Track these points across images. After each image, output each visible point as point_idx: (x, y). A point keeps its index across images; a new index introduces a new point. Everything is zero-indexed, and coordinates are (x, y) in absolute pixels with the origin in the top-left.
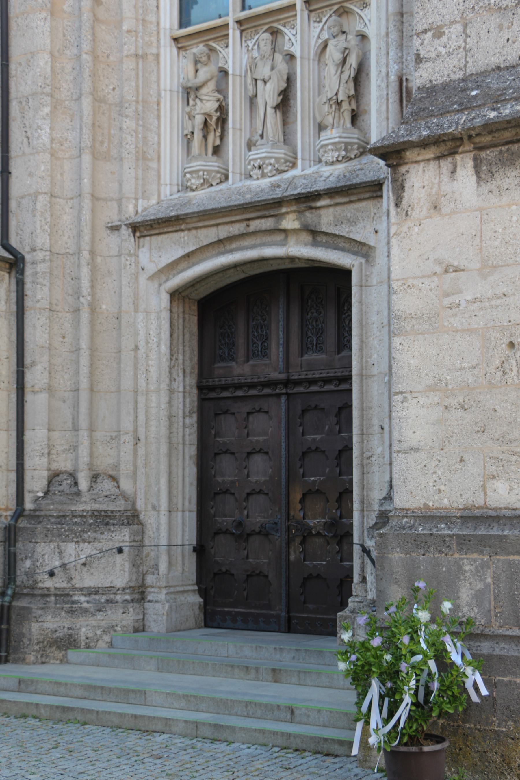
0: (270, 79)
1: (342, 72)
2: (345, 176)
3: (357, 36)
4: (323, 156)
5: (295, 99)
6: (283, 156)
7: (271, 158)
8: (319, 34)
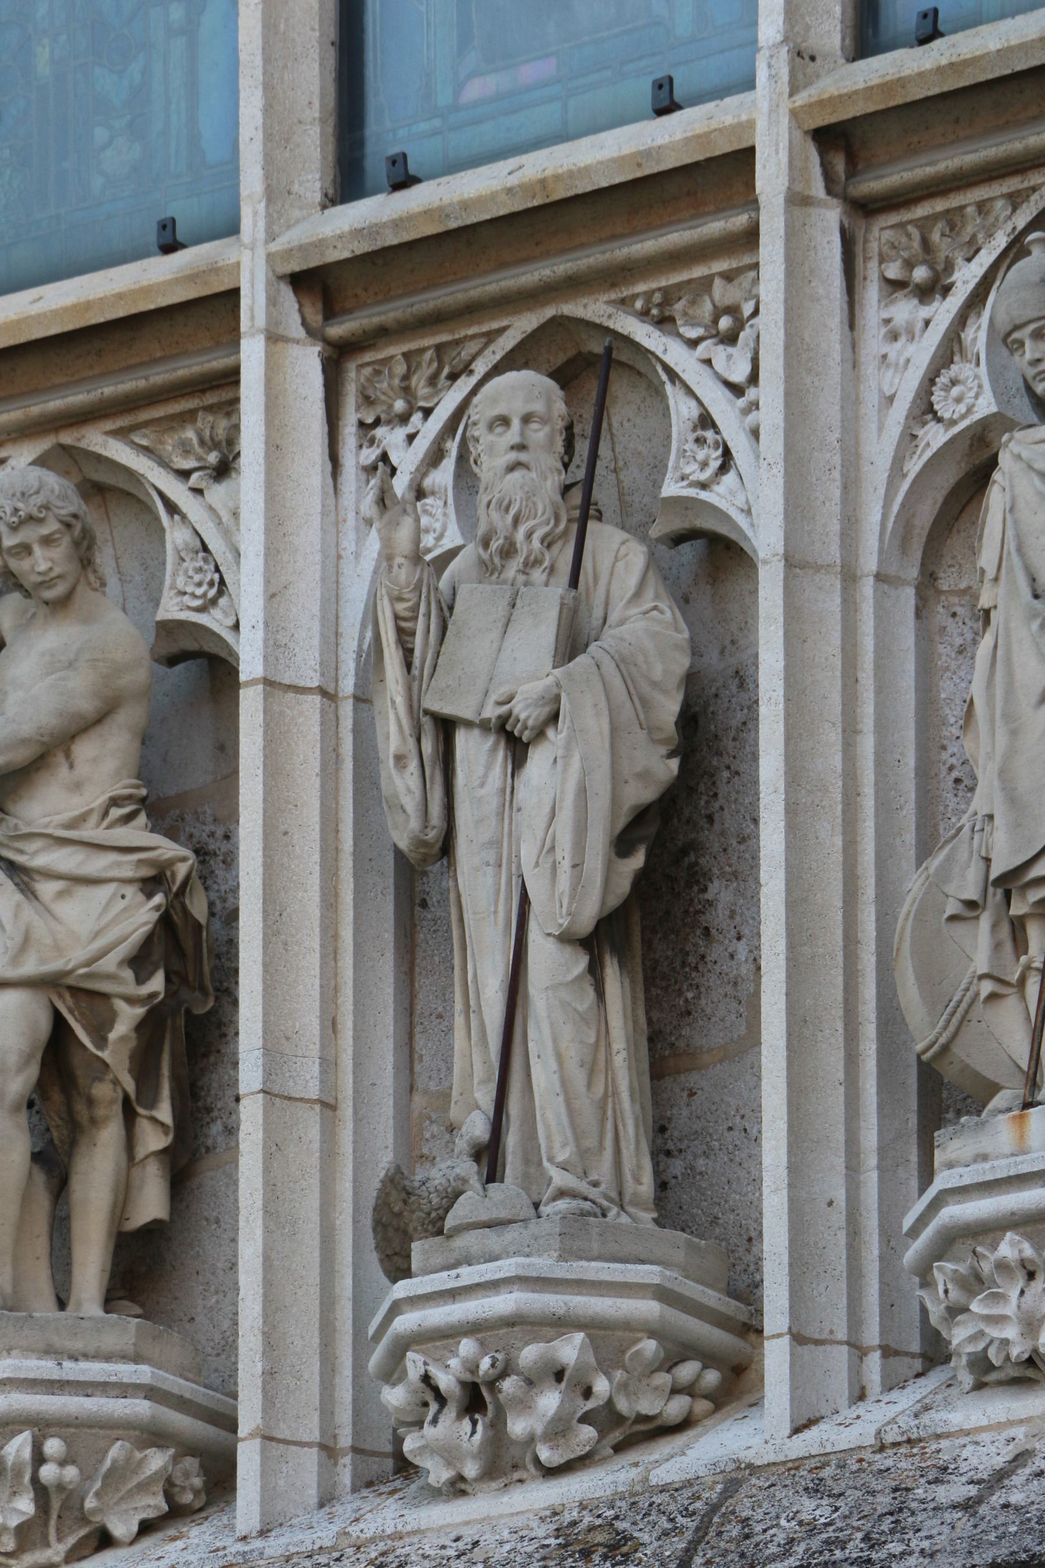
0: (554, 718)
4: (955, 1311)
5: (745, 876)
6: (648, 1308)
7: (561, 1324)
8: (930, 380)
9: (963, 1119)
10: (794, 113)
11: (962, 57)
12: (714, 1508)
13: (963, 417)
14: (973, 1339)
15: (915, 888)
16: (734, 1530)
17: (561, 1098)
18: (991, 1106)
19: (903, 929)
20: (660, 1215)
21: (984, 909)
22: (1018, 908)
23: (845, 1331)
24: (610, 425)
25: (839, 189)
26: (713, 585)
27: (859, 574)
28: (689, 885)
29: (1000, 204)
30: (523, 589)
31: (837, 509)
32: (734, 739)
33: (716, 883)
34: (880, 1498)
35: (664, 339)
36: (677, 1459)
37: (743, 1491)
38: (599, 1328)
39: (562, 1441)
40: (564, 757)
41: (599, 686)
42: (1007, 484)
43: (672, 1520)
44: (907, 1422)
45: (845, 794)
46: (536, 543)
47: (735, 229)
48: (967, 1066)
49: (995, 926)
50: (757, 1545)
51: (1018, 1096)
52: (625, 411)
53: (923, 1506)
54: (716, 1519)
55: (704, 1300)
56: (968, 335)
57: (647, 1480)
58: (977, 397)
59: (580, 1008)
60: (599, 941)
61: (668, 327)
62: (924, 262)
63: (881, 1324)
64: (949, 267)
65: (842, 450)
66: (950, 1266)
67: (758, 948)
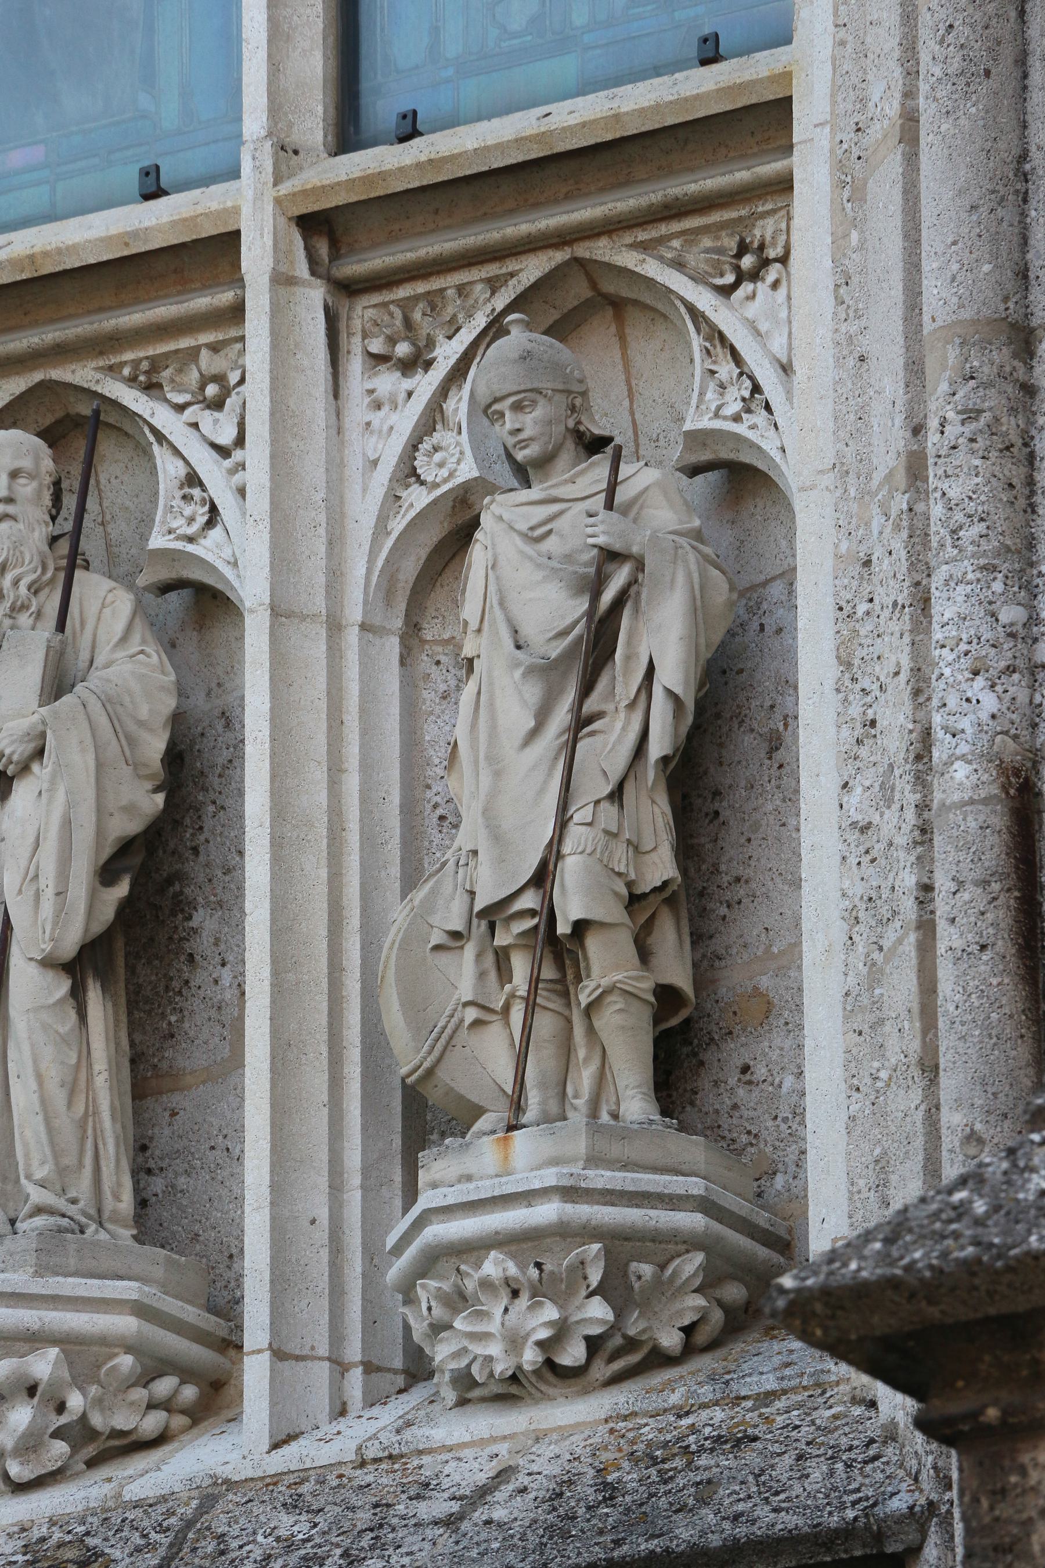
0: (39, 753)
1: (581, 722)
2: (610, 1492)
3: (694, 471)
4: (438, 1328)
5: (230, 905)
6: (126, 1324)
7: (34, 1340)
8: (413, 446)
9: (447, 1141)
10: (278, 201)
11: (440, 155)
12: (189, 1524)
13: (445, 481)
14: (456, 1355)
15: (400, 919)
16: (210, 1546)
17: (40, 1117)
18: (475, 1128)
19: (388, 958)
20: (140, 1232)
21: (468, 940)
22: (502, 939)
23: (327, 1347)
24: (98, 482)
25: (322, 270)
26: (200, 631)
27: (344, 623)
28: (173, 914)
29: (479, 287)
30: (9, 633)
31: (324, 562)
32: (220, 776)
33: (201, 911)
34: (360, 1514)
35: (151, 404)
36: (152, 1474)
37: (219, 1507)
38: (70, 1343)
39: (33, 1456)
40: (48, 790)
41: (86, 724)
42: (489, 544)
43: (145, 1536)
44: (388, 1438)
45: (330, 829)
46: (23, 589)
47: (221, 305)
48: (452, 1089)
49: (479, 956)
50: (233, 1561)
51: (502, 1119)
52: (113, 469)
53: (404, 1522)
54: (190, 1535)
55: (183, 1316)
56: (449, 406)
57: (121, 1495)
58: (458, 462)
59: (61, 1030)
60: (82, 966)
61: (155, 392)
62: (406, 338)
63: (363, 1341)
64: (431, 343)
65: (327, 508)
66: (433, 1284)
67: (243, 974)
